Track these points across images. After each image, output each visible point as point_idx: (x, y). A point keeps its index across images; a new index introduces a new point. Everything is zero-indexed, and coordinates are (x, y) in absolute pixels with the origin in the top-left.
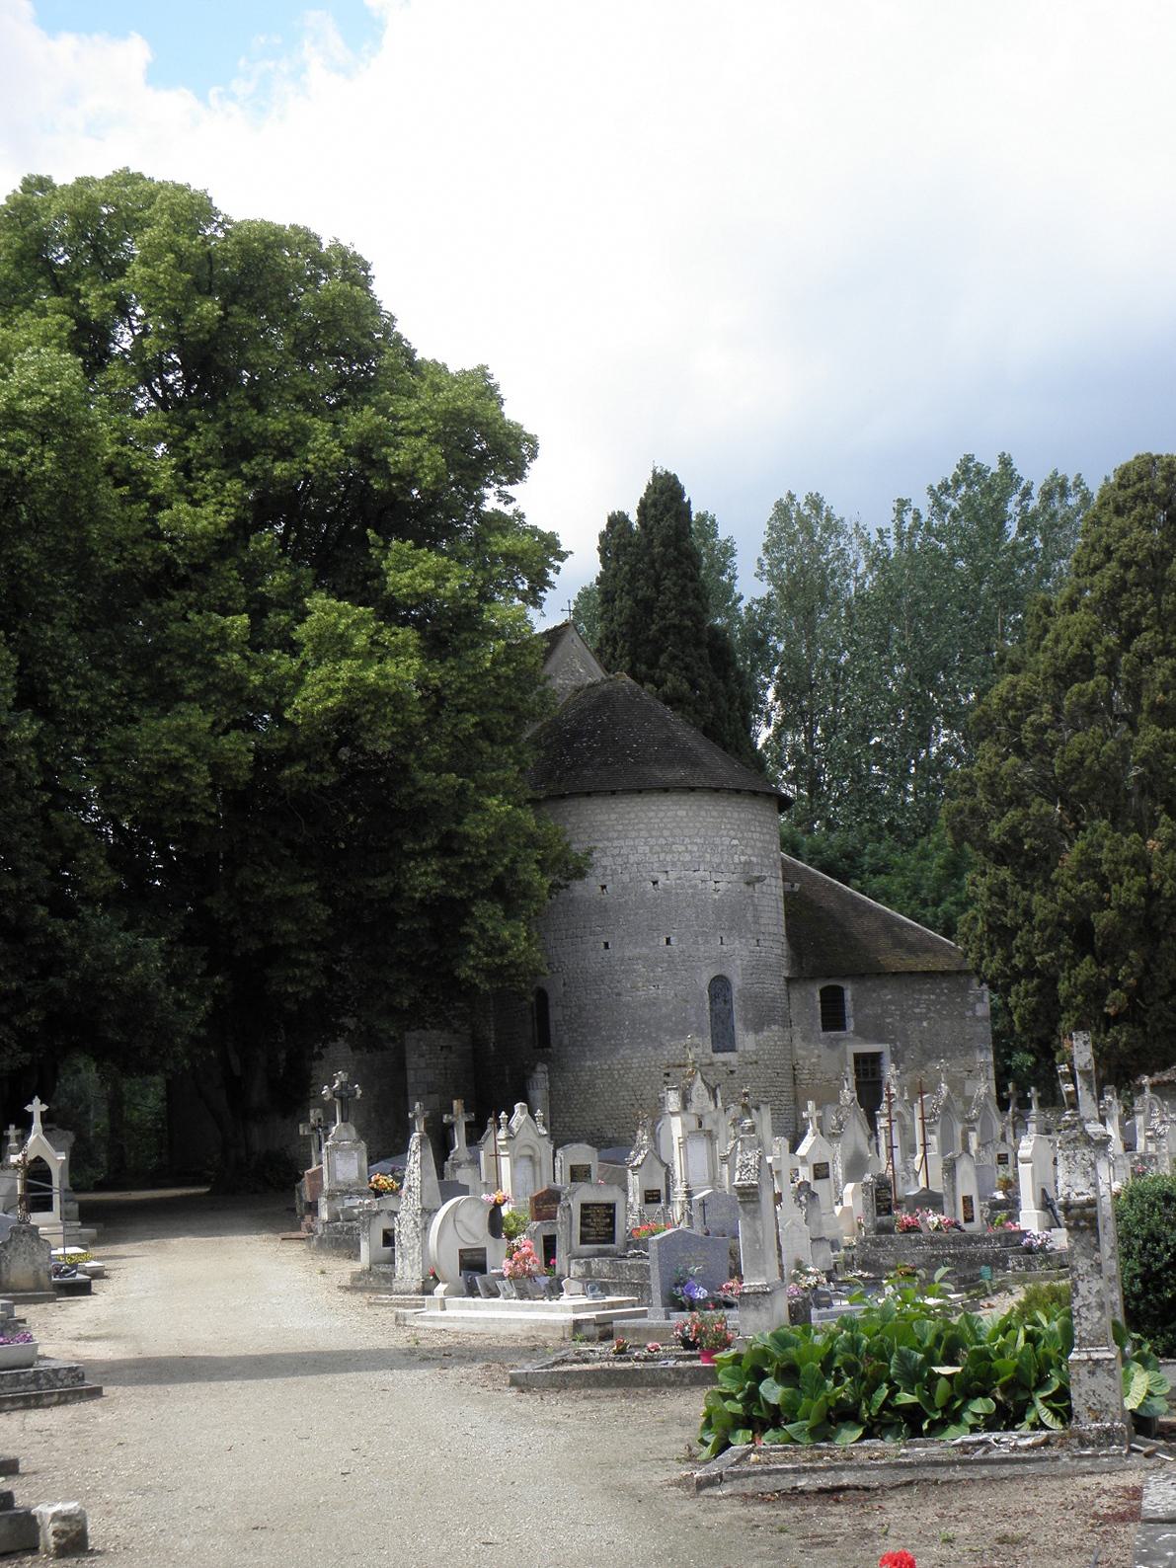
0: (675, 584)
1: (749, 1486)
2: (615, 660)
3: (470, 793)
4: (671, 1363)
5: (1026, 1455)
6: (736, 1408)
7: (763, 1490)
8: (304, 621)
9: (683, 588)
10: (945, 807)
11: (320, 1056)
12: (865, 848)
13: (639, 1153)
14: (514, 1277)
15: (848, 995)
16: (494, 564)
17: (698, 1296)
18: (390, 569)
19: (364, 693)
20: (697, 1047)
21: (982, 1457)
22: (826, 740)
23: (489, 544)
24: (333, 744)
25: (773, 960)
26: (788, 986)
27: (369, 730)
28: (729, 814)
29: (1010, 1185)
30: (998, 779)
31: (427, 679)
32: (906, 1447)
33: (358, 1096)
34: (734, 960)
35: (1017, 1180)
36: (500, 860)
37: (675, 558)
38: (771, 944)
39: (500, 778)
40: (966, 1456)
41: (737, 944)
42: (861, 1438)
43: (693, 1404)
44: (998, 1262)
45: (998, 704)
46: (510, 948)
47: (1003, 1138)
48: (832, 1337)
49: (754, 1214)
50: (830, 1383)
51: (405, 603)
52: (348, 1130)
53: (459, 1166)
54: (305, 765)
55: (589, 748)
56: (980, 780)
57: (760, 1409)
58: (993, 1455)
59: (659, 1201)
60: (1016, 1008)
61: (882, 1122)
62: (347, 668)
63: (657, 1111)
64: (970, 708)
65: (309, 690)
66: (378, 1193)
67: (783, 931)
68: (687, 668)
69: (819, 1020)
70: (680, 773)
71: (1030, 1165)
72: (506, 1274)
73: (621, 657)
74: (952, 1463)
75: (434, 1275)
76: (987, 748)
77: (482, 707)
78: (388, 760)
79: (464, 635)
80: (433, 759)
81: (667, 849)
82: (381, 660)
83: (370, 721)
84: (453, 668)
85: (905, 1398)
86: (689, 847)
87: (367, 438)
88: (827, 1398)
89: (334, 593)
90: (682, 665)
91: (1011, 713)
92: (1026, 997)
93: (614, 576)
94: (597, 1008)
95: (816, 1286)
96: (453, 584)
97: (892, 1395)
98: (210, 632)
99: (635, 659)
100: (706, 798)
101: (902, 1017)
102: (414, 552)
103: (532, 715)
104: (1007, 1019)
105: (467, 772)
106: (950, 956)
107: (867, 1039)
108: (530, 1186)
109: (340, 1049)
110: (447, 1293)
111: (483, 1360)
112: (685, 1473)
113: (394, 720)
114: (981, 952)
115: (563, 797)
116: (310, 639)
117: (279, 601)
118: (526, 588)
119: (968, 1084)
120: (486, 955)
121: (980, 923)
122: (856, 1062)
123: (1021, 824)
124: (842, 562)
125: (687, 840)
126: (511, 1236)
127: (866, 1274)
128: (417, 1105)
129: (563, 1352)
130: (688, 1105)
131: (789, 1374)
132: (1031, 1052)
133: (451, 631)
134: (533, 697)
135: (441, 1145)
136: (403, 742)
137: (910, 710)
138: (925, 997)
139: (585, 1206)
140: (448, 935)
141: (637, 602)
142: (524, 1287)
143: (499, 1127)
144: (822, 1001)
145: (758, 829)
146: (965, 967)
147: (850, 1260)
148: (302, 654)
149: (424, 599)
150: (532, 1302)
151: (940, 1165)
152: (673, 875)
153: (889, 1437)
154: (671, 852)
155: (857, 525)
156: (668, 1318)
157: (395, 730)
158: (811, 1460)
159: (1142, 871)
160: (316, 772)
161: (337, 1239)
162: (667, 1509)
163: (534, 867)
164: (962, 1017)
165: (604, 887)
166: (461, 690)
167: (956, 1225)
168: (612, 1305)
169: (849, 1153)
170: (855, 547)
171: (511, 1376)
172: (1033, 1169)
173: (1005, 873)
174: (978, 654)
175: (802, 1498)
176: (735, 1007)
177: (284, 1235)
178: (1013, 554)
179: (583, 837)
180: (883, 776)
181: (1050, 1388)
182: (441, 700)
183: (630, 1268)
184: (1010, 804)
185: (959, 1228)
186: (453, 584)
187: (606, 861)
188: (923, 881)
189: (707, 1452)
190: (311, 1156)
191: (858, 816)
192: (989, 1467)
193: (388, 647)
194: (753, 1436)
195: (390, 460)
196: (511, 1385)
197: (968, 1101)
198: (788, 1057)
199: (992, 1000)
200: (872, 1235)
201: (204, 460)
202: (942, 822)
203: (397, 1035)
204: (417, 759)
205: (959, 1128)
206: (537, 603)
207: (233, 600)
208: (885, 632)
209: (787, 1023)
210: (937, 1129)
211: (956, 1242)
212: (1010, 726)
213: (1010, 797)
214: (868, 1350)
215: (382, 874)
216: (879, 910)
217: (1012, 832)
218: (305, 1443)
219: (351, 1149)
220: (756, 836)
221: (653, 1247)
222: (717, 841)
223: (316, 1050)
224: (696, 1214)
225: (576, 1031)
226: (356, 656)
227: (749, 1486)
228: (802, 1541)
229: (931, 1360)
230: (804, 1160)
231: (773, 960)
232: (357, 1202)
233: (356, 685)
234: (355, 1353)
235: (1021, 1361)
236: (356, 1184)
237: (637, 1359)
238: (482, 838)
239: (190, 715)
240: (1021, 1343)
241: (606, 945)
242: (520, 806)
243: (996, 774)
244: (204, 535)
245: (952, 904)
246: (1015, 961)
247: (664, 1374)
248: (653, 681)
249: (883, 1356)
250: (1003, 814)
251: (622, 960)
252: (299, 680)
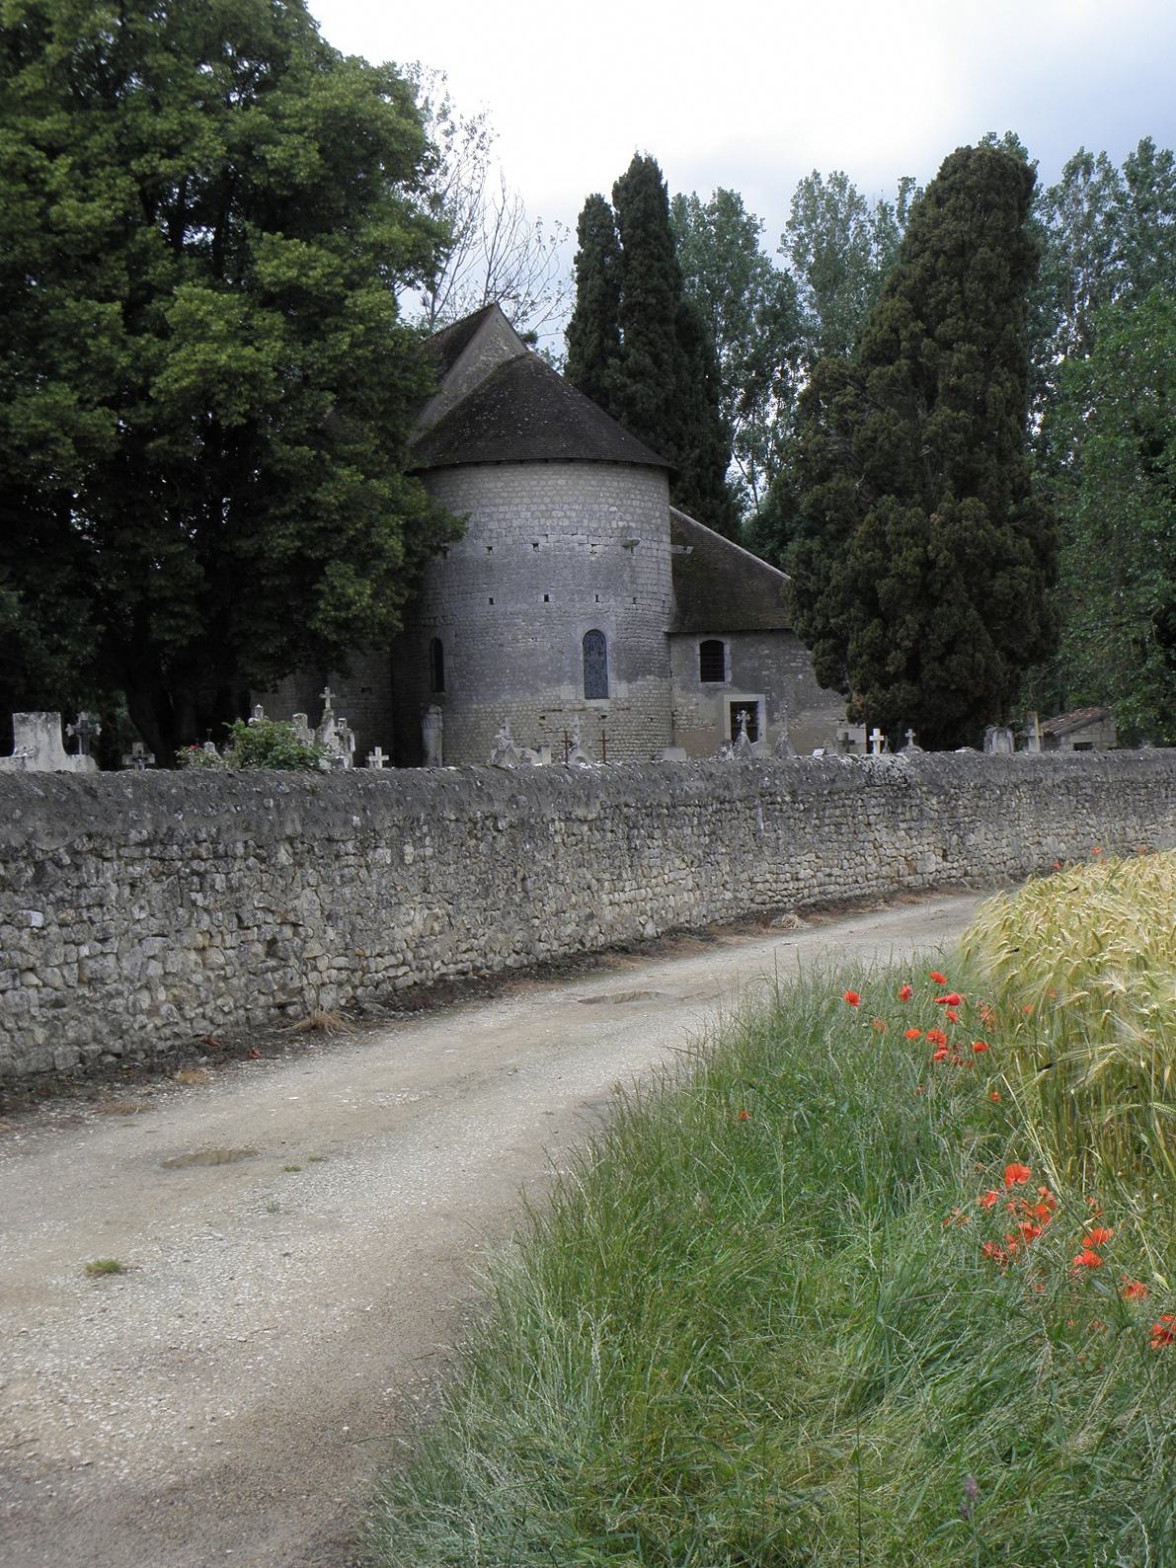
9: (649, 268)
15: (727, 649)
25: (650, 616)
28: (608, 483)
38: (649, 602)
55: (488, 420)
68: (651, 343)
69: (699, 672)
73: (591, 332)
81: (547, 514)
87: (249, 136)
90: (645, 340)
98: (84, 318)
100: (586, 468)
101: (779, 669)
107: (743, 689)
138: (801, 652)
141: (607, 282)
144: (702, 654)
145: (638, 497)
152: (552, 538)
159: (920, 543)
165: (490, 548)
166: (322, 371)
176: (608, 658)
187: (493, 525)
195: (268, 157)
201: (100, 158)
207: (118, 288)
209: (664, 672)
215: (249, 537)
216: (771, 572)
222: (596, 507)
226: (215, 339)
231: (650, 616)
239: (57, 394)
241: (491, 600)
244: (89, 227)
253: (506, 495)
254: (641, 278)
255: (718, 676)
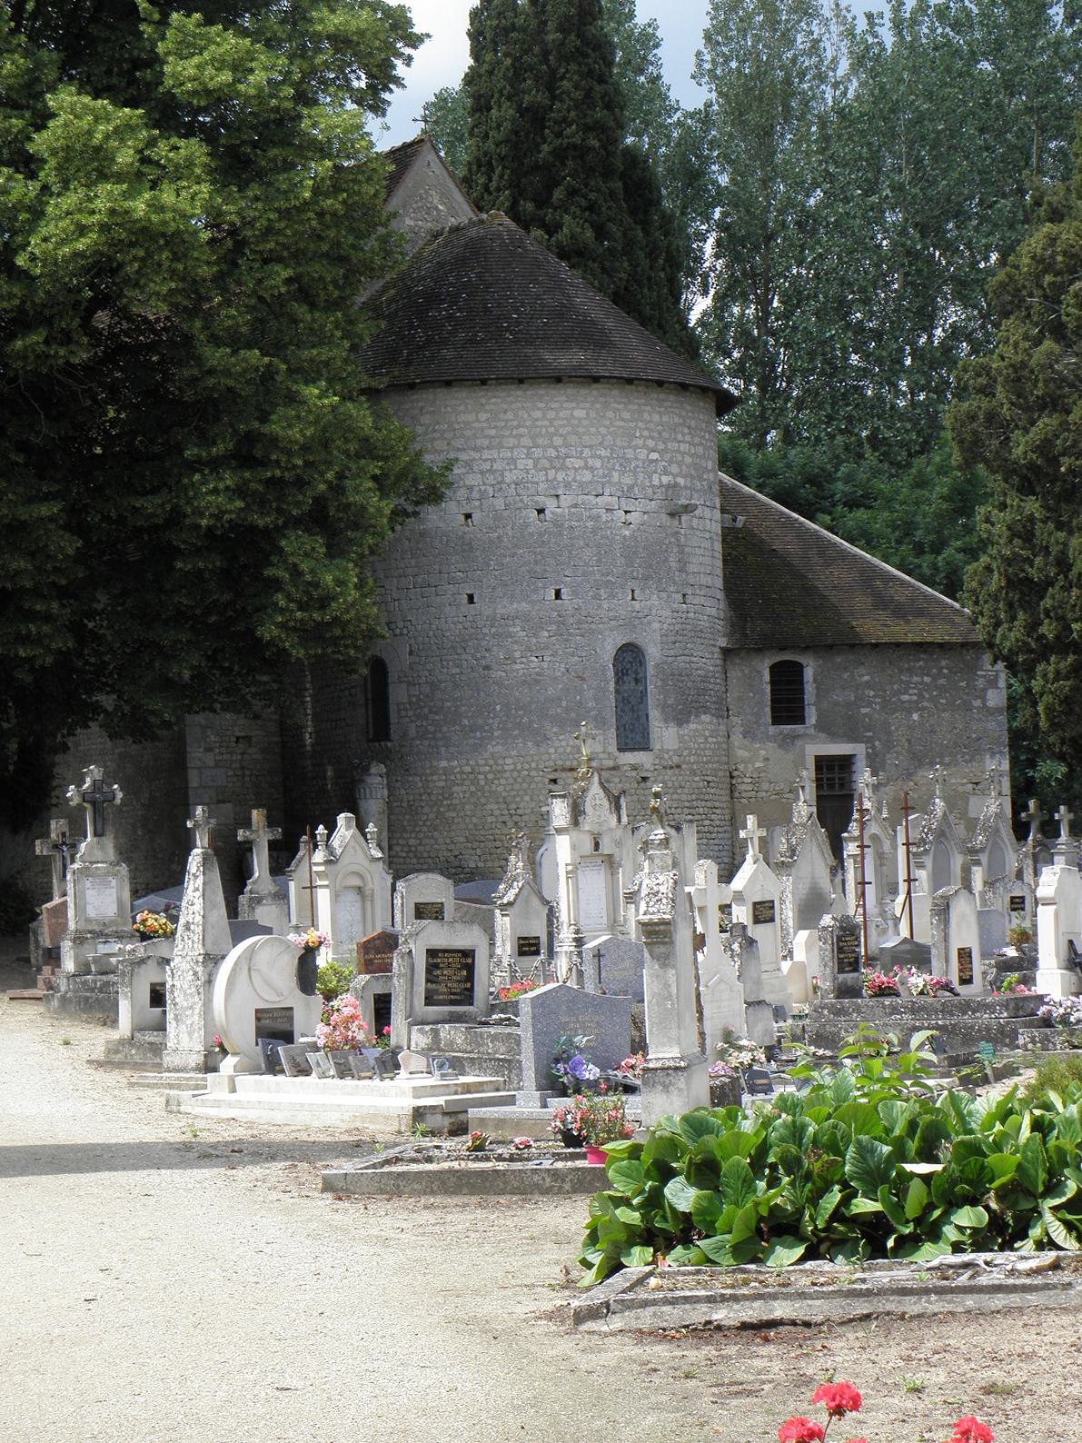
0: (576, 87)
1: (646, 1319)
2: (490, 193)
3: (279, 378)
4: (547, 1164)
5: (1028, 1281)
6: (633, 1217)
7: (665, 1325)
8: (45, 127)
10: (949, 412)
11: (65, 748)
12: (837, 470)
13: (511, 886)
14: (332, 1049)
15: (809, 674)
16: (318, 50)
17: (587, 1076)
18: (168, 53)
19: (131, 232)
20: (596, 743)
21: (967, 1283)
22: (786, 316)
23: (310, 21)
24: (85, 304)
25: (704, 624)
26: (724, 660)
27: (136, 285)
28: (646, 416)
29: (1026, 939)
30: (1026, 373)
31: (220, 214)
32: (864, 1270)
33: (118, 801)
34: (649, 623)
35: (1036, 934)
36: (322, 474)
37: (578, 50)
38: (702, 600)
39: (324, 358)
40: (945, 1283)
41: (654, 600)
42: (802, 1259)
43: (575, 1216)
44: (1005, 1037)
45: (1029, 265)
46: (334, 598)
47: (1019, 875)
48: (767, 1123)
49: (665, 960)
50: (762, 1185)
51: (190, 103)
52: (102, 848)
53: (259, 901)
54: (45, 333)
55: (450, 317)
56: (1000, 374)
57: (664, 1218)
58: (983, 1280)
59: (537, 953)
60: (1042, 695)
61: (851, 848)
62: (105, 196)
63: (539, 831)
64: (989, 272)
65: (52, 226)
66: (144, 937)
67: (719, 583)
68: (591, 207)
69: (768, 709)
70: (575, 357)
71: (1054, 907)
72: (321, 1043)
73: (498, 190)
74: (926, 1291)
75: (221, 1046)
76: (1013, 328)
77: (298, 256)
78: (165, 329)
79: (273, 152)
80: (227, 329)
81: (559, 463)
82: (154, 185)
83: (137, 272)
84: (257, 199)
85: (863, 1206)
86: (590, 462)
88: (757, 1204)
89: (88, 88)
90: (584, 203)
91: (1048, 279)
92: (1057, 678)
93: (491, 73)
94: (456, 686)
95: (750, 1065)
96: (258, 77)
97: (846, 1201)
99: (518, 192)
100: (615, 392)
102: (203, 30)
103: (370, 270)
104: (1029, 712)
105: (276, 348)
106: (952, 622)
107: (834, 736)
108: (358, 929)
109: (92, 736)
110: (239, 1069)
111: (286, 1159)
112: (559, 1303)
113: (173, 272)
114: (996, 616)
115: (412, 386)
116: (54, 152)
117: (8, 97)
118: (363, 86)
119: (973, 800)
120: (301, 608)
121: (996, 576)
122: (818, 768)
123: (1057, 437)
124: (815, 60)
125: (587, 452)
126: (329, 996)
127: (821, 1052)
128: (199, 810)
129: (398, 1149)
130: (581, 819)
131: (706, 1172)
132: (1061, 757)
133: (255, 145)
134: (371, 244)
135: (235, 874)
136: (186, 303)
137: (907, 274)
138: (915, 679)
139: (432, 953)
140: (247, 579)
141: (522, 111)
142: (346, 1061)
143: (316, 846)
144: (773, 682)
145: (688, 438)
146: (972, 638)
147: (799, 1032)
148: (42, 174)
149: (218, 99)
150: (356, 1082)
151: (928, 905)
152: (566, 501)
153: (840, 1257)
154: (564, 468)
155: (837, 5)
156: (545, 1106)
157: (173, 285)
158: (733, 1287)
160: (61, 344)
161: (87, 999)
162: (533, 1349)
163: (370, 484)
164: (968, 707)
165: (468, 516)
166: (268, 231)
167: (947, 987)
168: (468, 1088)
169: (803, 890)
170: (835, 38)
171: (325, 1178)
172: (1056, 914)
173: (1033, 506)
174: (1004, 196)
175: (718, 1336)
176: (650, 688)
177: (12, 993)
178: (1056, 53)
179: (440, 445)
180: (865, 369)
181: (1064, 1194)
182: (240, 245)
183: (494, 1038)
184: (1042, 409)
185: (951, 990)
186: (258, 77)
187: (473, 480)
188: (919, 519)
189: (590, 1276)
190: (51, 888)
191: (828, 424)
192: (975, 1296)
193: (164, 167)
194: (654, 1256)
196: (324, 1190)
197: (972, 825)
198: (725, 759)
199: (1010, 686)
200: (831, 999)
202: (948, 435)
203: (173, 719)
204: (205, 328)
205: (958, 861)
206: (379, 108)
208: (875, 163)
209: (723, 712)
210: (928, 861)
211: (946, 1010)
212: (1045, 297)
213: (1043, 398)
214: (815, 1142)
215: (154, 491)
217: (1044, 447)
218: (36, 1261)
219: (107, 874)
220: (684, 447)
221: (525, 1009)
222: (630, 454)
223: (59, 739)
224: (589, 969)
225: (427, 719)
226: (119, 178)
227: (646, 1319)
228: (715, 1390)
229: (900, 1155)
230: (739, 897)
232: (116, 947)
233: (119, 220)
234: (107, 1148)
235: (1025, 1157)
236: (113, 923)
237: (500, 1158)
238: (296, 442)
240: (1026, 1133)
241: (471, 599)
242: (351, 399)
243: (1024, 365)
245: (959, 550)
246: (1043, 629)
247: (536, 1178)
248: (543, 225)
249: (835, 1147)
250: (1033, 423)
251: (492, 620)
252: (37, 213)
253: (493, 432)
254: (576, 107)
255: (799, 718)
